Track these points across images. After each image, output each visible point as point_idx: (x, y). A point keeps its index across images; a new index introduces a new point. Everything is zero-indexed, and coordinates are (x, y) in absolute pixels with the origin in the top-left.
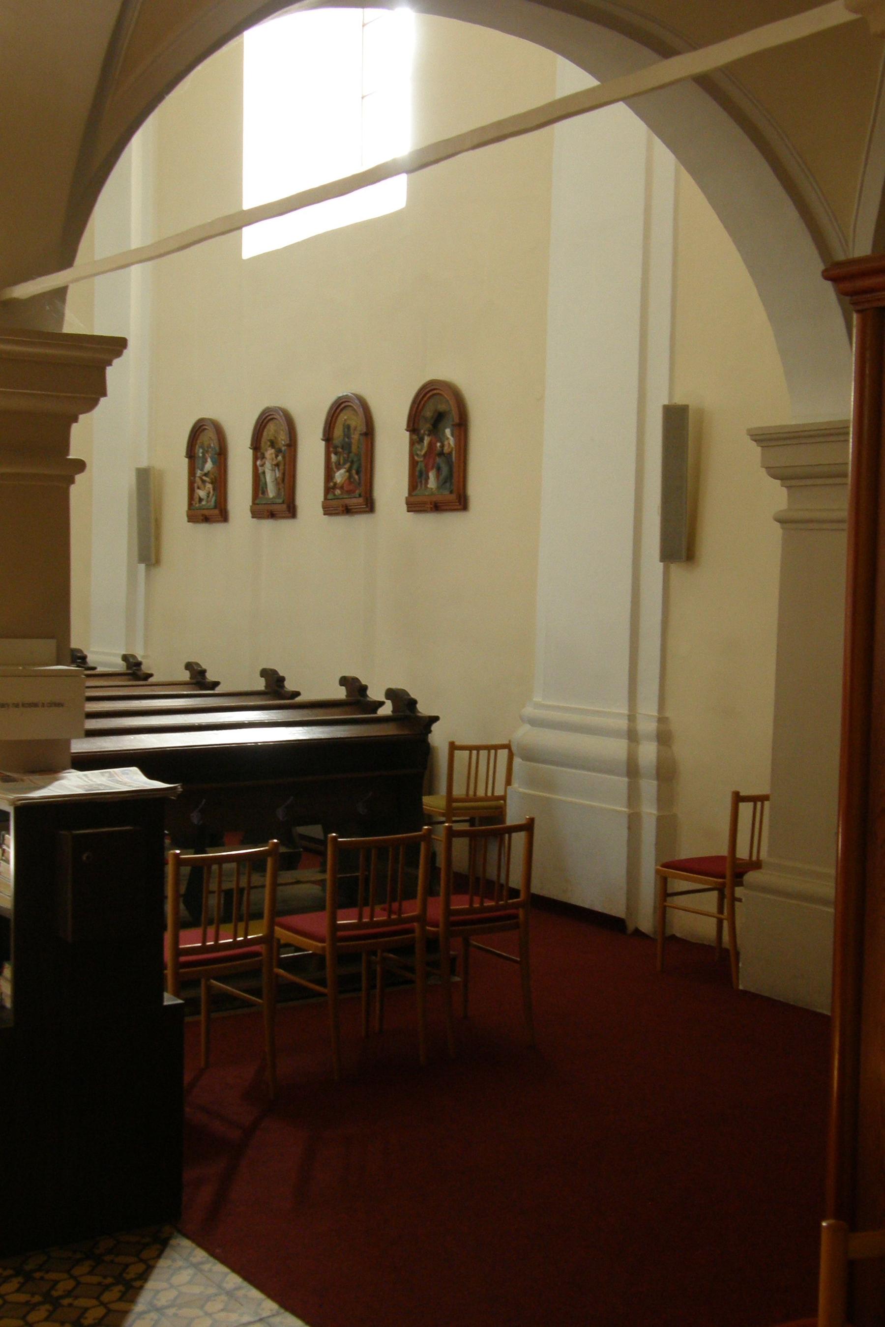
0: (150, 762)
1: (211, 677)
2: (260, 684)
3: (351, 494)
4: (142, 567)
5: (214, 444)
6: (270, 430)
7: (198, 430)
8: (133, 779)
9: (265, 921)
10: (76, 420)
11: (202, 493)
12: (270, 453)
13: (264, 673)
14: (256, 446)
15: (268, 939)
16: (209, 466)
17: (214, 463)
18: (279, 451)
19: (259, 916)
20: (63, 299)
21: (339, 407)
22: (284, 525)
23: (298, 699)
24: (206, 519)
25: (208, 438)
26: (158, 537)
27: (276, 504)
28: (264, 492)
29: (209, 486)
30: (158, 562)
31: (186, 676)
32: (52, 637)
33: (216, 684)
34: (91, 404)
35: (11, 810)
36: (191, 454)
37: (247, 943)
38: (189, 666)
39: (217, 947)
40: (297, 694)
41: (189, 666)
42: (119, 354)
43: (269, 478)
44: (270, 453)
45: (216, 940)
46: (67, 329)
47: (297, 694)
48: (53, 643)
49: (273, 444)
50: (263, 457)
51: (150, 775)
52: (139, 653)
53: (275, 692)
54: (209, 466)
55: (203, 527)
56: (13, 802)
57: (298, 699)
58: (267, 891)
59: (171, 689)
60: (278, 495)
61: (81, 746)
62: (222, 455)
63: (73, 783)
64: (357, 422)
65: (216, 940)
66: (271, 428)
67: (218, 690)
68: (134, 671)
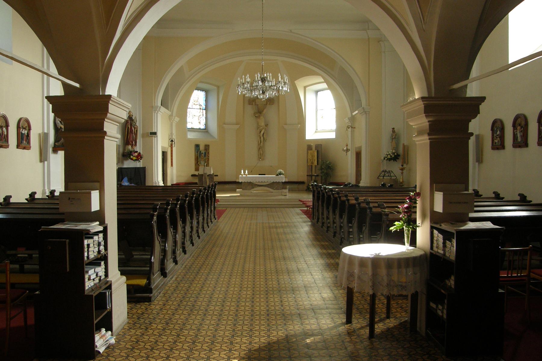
0: (493, 220)
1: (501, 196)
2: (518, 198)
3: (521, 143)
4: (477, 163)
5: (500, 126)
6: (519, 121)
7: (495, 122)
8: (489, 225)
9: (527, 271)
10: (470, 121)
11: (496, 141)
12: (519, 128)
13: (519, 195)
14: (514, 126)
15: (528, 276)
16: (498, 133)
17: (500, 131)
18: (522, 127)
19: (526, 269)
20: (466, 87)
21: (517, 118)
22: (502, 151)
23: (531, 203)
24: (498, 149)
25: (498, 124)
26: (482, 155)
27: (521, 143)
28: (517, 139)
29: (498, 139)
30: (482, 162)
31: (493, 196)
32: (98, 182)
33: (503, 198)
34: (475, 116)
35: (455, 232)
36: (492, 129)
37: (521, 276)
38: (494, 193)
39: (512, 277)
40: (531, 201)
41: (494, 193)
42: (483, 101)
43: (519, 135)
44: (519, 128)
45: (512, 274)
46: (468, 96)
47: (531, 201)
48: (464, 185)
49: (520, 125)
50: (516, 129)
51: (494, 223)
52: (476, 188)
53: (522, 201)
54: (498, 133)
55: (496, 151)
56: (455, 230)
57: (531, 203)
58: (528, 261)
59: (488, 199)
60: (522, 140)
61: (472, 215)
62: (502, 129)
63: (471, 225)
64: (499, 123)
65: (512, 274)
66: (519, 120)
67: (504, 200)
68: (476, 193)
